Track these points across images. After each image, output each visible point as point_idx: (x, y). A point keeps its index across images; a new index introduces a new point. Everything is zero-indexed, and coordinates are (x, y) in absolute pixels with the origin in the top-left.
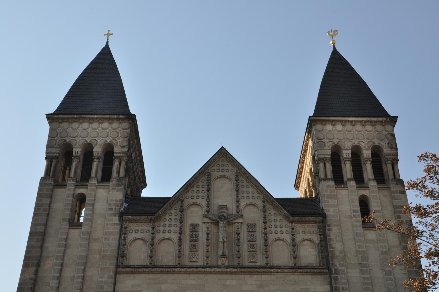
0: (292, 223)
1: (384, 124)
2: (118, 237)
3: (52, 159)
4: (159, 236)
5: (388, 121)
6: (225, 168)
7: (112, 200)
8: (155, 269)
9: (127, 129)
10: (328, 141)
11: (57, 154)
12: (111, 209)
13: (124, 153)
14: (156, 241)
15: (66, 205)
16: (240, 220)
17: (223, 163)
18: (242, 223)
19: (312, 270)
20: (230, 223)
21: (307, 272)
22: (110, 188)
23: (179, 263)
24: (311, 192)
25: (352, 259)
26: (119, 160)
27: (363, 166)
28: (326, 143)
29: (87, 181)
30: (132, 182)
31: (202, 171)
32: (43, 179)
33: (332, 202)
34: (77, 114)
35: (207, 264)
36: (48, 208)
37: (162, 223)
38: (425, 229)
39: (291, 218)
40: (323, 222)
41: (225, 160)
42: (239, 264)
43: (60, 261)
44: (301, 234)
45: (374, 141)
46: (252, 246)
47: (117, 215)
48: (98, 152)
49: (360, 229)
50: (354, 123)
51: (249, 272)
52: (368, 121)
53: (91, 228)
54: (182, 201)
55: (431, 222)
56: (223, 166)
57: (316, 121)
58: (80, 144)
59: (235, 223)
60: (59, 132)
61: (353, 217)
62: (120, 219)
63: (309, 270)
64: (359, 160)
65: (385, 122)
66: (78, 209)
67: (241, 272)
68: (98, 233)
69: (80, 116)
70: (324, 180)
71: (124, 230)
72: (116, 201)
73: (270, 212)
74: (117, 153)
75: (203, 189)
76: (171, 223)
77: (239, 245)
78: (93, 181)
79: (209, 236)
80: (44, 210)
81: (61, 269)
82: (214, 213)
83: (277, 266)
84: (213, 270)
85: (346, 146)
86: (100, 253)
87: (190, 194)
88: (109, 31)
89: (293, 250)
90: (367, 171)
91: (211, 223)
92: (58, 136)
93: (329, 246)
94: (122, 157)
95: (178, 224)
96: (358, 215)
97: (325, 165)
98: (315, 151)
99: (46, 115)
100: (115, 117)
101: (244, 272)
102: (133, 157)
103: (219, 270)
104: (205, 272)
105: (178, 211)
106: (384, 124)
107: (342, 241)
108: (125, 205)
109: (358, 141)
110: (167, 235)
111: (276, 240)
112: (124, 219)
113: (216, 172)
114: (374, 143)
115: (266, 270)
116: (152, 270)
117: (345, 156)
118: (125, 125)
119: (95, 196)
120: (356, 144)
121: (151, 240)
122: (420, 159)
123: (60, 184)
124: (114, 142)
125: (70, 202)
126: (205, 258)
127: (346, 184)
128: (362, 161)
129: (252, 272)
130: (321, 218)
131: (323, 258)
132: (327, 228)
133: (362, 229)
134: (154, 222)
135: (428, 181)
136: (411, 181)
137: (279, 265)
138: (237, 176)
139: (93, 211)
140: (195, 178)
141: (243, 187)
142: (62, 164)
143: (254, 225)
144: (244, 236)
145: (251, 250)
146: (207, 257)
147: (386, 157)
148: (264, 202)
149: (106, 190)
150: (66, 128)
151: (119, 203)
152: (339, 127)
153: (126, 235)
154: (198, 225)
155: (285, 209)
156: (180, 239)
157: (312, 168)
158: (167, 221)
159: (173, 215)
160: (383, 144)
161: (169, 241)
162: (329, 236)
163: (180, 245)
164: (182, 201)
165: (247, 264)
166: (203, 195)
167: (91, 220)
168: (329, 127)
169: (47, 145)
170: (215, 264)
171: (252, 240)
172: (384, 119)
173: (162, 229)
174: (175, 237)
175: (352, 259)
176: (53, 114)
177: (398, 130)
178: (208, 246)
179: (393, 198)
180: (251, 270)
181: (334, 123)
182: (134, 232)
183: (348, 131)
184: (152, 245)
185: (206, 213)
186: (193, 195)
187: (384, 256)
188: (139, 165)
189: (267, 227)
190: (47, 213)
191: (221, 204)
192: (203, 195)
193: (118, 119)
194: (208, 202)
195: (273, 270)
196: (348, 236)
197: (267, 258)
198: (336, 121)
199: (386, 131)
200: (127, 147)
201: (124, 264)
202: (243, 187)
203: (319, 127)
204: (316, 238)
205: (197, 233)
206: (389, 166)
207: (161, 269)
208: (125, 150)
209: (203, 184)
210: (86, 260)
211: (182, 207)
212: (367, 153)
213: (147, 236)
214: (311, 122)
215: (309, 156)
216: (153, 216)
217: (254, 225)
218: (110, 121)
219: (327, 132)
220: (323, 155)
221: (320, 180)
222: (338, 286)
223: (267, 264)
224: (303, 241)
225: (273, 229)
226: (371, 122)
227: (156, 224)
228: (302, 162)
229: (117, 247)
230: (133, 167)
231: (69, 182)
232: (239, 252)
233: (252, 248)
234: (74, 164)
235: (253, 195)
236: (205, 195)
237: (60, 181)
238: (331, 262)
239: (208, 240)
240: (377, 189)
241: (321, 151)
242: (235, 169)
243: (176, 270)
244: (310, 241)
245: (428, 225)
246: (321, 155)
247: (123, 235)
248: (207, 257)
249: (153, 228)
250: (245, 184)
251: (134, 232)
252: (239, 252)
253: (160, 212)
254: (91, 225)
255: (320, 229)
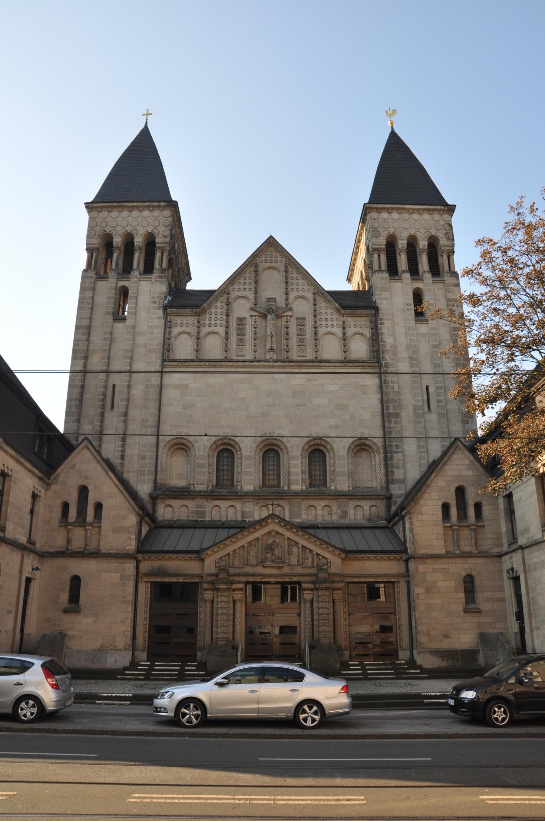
0: (343, 317)
1: (441, 213)
2: (162, 330)
3: (92, 250)
4: (205, 330)
5: (446, 210)
6: (274, 259)
7: (156, 293)
8: (202, 363)
9: (168, 217)
10: (383, 230)
11: (98, 245)
12: (155, 302)
13: (166, 243)
14: (202, 335)
15: (109, 298)
16: (289, 313)
17: (271, 253)
18: (291, 316)
19: (362, 364)
20: (278, 317)
21: (357, 366)
22: (153, 280)
23: (226, 358)
24: (364, 285)
25: (403, 353)
26: (161, 251)
27: (419, 257)
28: (381, 232)
29: (129, 273)
30: (176, 274)
31: (249, 262)
32: (85, 271)
33: (385, 295)
34: (116, 202)
35: (255, 358)
36: (91, 301)
37: (207, 316)
38: (477, 318)
39: (343, 311)
40: (375, 315)
41: (274, 250)
42: (287, 358)
43: (107, 355)
44: (352, 328)
45: (430, 231)
46: (301, 340)
47: (161, 308)
48: (139, 242)
49: (412, 323)
50: (411, 211)
51: (298, 366)
52: (426, 209)
53: (136, 321)
54: (228, 294)
55: (482, 311)
56: (271, 256)
57: (372, 208)
58: (120, 234)
59: (284, 316)
60: (98, 222)
61: (406, 310)
62: (164, 312)
63: (358, 364)
64: (415, 252)
65: (443, 210)
66: (122, 303)
67: (290, 366)
68: (142, 327)
69: (119, 204)
70: (378, 271)
71: (168, 323)
72: (160, 293)
73: (320, 305)
74: (159, 243)
75: (250, 281)
76: (217, 316)
77: (287, 339)
78: (135, 273)
79: (257, 329)
80: (88, 303)
81: (109, 362)
82: (262, 306)
83: (449, 459)
84: (261, 364)
85: (402, 236)
86: (146, 347)
87: (236, 286)
88: (148, 110)
89: (344, 344)
90: (422, 263)
91: (259, 316)
92: (98, 226)
93: (380, 340)
94: (165, 247)
95: (224, 317)
96: (411, 309)
97: (379, 256)
98: (370, 241)
99: (85, 203)
100: (156, 204)
101: (293, 366)
102: (176, 248)
103: (267, 364)
104: (252, 366)
105: (224, 304)
106: (441, 213)
107: (394, 335)
108: (169, 298)
109: (415, 230)
110: (213, 329)
111: (326, 334)
112: (168, 312)
113: (264, 263)
114: (431, 233)
115: (315, 364)
116: (199, 364)
117: (400, 246)
118: (167, 213)
119: (138, 288)
120: (412, 234)
121: (196, 334)
122: (477, 244)
123: (102, 277)
124: (156, 231)
125: (113, 295)
126: (253, 352)
127: (401, 276)
128: (418, 252)
129: (301, 366)
130: (373, 311)
131: (373, 352)
132: (379, 321)
133: (414, 322)
134: (199, 316)
135: (484, 267)
136: (467, 267)
137: (329, 359)
138: (286, 267)
139: (136, 304)
140: (242, 269)
141: (292, 278)
142: (103, 255)
143: (304, 319)
144: (293, 329)
145: (300, 344)
146: (255, 351)
147: (442, 248)
148: (314, 294)
149: (149, 282)
150: (105, 217)
151: (163, 296)
152: (395, 215)
153: (171, 329)
154: (246, 318)
155: (337, 302)
156: (227, 333)
157: (366, 260)
158: (213, 314)
159: (219, 308)
160: (439, 234)
161: (215, 335)
162: (381, 330)
163: (227, 339)
164: (228, 294)
165: (295, 358)
166: (250, 287)
167: (135, 314)
168: (385, 215)
169: (87, 236)
170: (263, 358)
171: (301, 334)
172: (442, 207)
173: (207, 322)
174: (221, 330)
175: (403, 353)
176: (92, 203)
177: (456, 220)
178: (255, 339)
179: (447, 291)
180: (300, 364)
181: (390, 211)
182: (179, 326)
183: (405, 220)
184: (198, 339)
185: (253, 306)
186: (240, 287)
187: (435, 349)
188: (183, 257)
189: (317, 321)
190: (91, 306)
191: (269, 297)
192: (250, 287)
193: (159, 206)
194: (256, 294)
195: (322, 364)
196: (400, 330)
197: (316, 352)
198: (392, 208)
199: (444, 220)
200: (169, 236)
201: (170, 358)
202: (292, 278)
203: (374, 215)
204: (367, 332)
205: (244, 327)
206: (445, 257)
207: (207, 363)
208: (168, 239)
209: (250, 275)
210: (132, 354)
211: (228, 299)
212: (423, 244)
213: (193, 330)
214: (366, 209)
215: (363, 248)
216: (198, 310)
217: (304, 319)
218: (151, 209)
219: (382, 220)
220: (378, 245)
221: (374, 272)
222: (387, 379)
223: (316, 358)
224: (354, 334)
225: (324, 323)
226: (429, 210)
227: (202, 317)
228: (355, 253)
229: (162, 341)
230: (176, 259)
231: (110, 274)
232: (287, 346)
233: (301, 342)
234: (115, 255)
235: (304, 287)
236: (252, 287)
237: (102, 273)
238: (381, 356)
239: (255, 334)
240: (432, 282)
241: (376, 241)
242: (284, 260)
243: (223, 363)
244: (361, 334)
245: (480, 315)
246: (375, 245)
247: (168, 329)
248: (255, 351)
249: (198, 322)
250: (295, 275)
251: (179, 326)
252: (287, 346)
253: (205, 305)
254: (135, 319)
255: (372, 323)
